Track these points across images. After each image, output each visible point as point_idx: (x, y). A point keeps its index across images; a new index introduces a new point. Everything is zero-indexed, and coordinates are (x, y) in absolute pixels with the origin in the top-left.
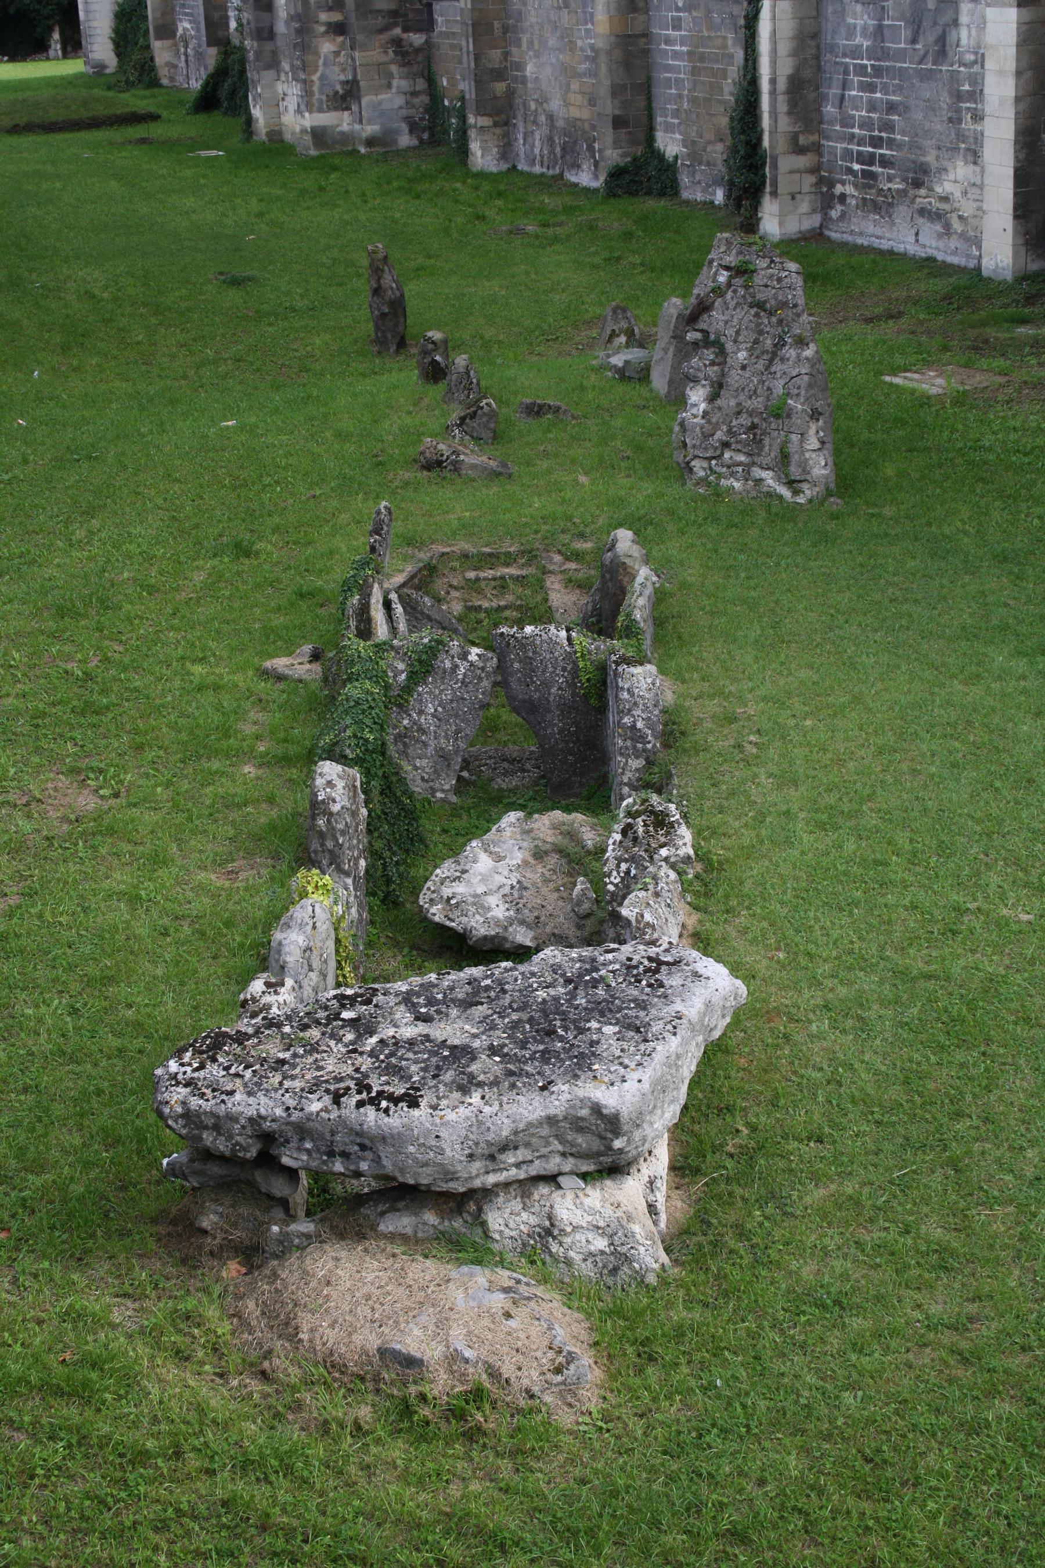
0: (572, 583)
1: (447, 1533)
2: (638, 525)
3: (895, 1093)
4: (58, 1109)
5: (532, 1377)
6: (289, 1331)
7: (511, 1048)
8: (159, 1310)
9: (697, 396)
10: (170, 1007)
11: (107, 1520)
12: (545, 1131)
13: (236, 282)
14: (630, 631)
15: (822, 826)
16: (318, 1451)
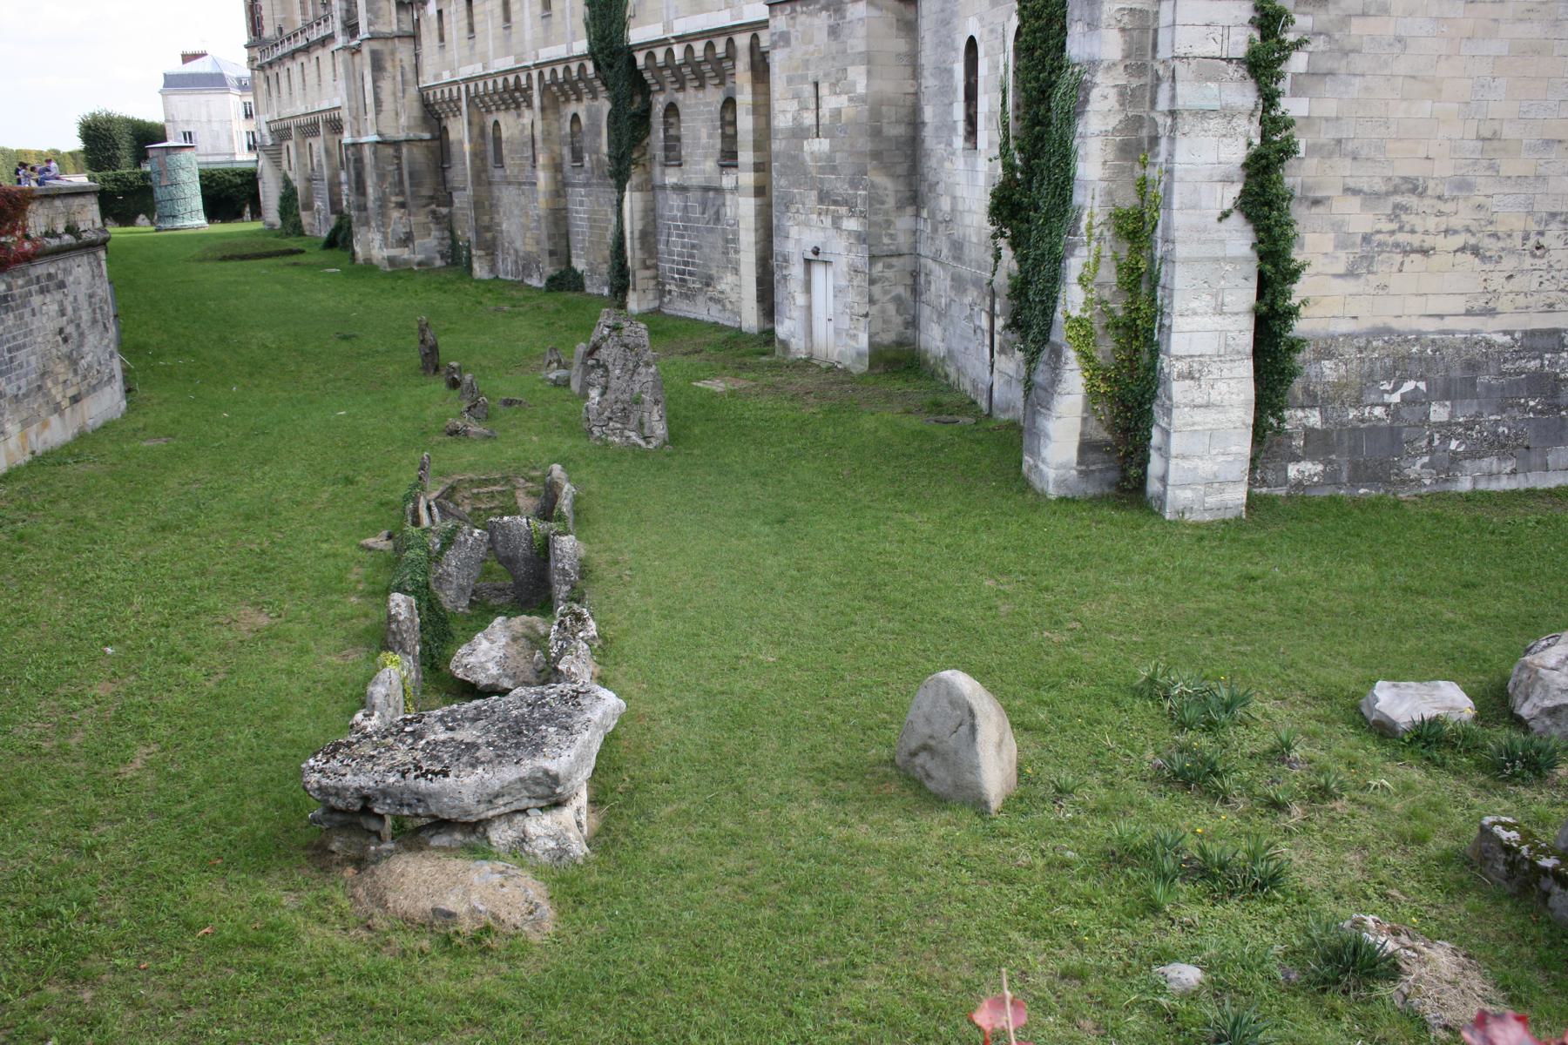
0: (529, 493)
1: (473, 1004)
2: (565, 462)
3: (706, 754)
4: (249, 790)
5: (517, 918)
6: (382, 903)
7: (499, 743)
8: (309, 896)
9: (594, 394)
10: (311, 731)
11: (282, 1012)
12: (519, 786)
13: (345, 338)
14: (561, 518)
15: (665, 617)
16: (401, 966)
